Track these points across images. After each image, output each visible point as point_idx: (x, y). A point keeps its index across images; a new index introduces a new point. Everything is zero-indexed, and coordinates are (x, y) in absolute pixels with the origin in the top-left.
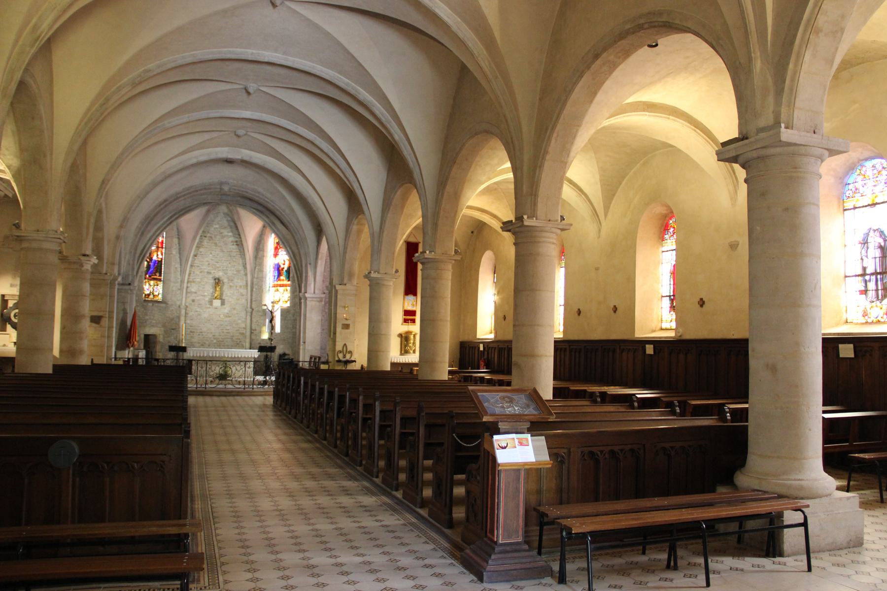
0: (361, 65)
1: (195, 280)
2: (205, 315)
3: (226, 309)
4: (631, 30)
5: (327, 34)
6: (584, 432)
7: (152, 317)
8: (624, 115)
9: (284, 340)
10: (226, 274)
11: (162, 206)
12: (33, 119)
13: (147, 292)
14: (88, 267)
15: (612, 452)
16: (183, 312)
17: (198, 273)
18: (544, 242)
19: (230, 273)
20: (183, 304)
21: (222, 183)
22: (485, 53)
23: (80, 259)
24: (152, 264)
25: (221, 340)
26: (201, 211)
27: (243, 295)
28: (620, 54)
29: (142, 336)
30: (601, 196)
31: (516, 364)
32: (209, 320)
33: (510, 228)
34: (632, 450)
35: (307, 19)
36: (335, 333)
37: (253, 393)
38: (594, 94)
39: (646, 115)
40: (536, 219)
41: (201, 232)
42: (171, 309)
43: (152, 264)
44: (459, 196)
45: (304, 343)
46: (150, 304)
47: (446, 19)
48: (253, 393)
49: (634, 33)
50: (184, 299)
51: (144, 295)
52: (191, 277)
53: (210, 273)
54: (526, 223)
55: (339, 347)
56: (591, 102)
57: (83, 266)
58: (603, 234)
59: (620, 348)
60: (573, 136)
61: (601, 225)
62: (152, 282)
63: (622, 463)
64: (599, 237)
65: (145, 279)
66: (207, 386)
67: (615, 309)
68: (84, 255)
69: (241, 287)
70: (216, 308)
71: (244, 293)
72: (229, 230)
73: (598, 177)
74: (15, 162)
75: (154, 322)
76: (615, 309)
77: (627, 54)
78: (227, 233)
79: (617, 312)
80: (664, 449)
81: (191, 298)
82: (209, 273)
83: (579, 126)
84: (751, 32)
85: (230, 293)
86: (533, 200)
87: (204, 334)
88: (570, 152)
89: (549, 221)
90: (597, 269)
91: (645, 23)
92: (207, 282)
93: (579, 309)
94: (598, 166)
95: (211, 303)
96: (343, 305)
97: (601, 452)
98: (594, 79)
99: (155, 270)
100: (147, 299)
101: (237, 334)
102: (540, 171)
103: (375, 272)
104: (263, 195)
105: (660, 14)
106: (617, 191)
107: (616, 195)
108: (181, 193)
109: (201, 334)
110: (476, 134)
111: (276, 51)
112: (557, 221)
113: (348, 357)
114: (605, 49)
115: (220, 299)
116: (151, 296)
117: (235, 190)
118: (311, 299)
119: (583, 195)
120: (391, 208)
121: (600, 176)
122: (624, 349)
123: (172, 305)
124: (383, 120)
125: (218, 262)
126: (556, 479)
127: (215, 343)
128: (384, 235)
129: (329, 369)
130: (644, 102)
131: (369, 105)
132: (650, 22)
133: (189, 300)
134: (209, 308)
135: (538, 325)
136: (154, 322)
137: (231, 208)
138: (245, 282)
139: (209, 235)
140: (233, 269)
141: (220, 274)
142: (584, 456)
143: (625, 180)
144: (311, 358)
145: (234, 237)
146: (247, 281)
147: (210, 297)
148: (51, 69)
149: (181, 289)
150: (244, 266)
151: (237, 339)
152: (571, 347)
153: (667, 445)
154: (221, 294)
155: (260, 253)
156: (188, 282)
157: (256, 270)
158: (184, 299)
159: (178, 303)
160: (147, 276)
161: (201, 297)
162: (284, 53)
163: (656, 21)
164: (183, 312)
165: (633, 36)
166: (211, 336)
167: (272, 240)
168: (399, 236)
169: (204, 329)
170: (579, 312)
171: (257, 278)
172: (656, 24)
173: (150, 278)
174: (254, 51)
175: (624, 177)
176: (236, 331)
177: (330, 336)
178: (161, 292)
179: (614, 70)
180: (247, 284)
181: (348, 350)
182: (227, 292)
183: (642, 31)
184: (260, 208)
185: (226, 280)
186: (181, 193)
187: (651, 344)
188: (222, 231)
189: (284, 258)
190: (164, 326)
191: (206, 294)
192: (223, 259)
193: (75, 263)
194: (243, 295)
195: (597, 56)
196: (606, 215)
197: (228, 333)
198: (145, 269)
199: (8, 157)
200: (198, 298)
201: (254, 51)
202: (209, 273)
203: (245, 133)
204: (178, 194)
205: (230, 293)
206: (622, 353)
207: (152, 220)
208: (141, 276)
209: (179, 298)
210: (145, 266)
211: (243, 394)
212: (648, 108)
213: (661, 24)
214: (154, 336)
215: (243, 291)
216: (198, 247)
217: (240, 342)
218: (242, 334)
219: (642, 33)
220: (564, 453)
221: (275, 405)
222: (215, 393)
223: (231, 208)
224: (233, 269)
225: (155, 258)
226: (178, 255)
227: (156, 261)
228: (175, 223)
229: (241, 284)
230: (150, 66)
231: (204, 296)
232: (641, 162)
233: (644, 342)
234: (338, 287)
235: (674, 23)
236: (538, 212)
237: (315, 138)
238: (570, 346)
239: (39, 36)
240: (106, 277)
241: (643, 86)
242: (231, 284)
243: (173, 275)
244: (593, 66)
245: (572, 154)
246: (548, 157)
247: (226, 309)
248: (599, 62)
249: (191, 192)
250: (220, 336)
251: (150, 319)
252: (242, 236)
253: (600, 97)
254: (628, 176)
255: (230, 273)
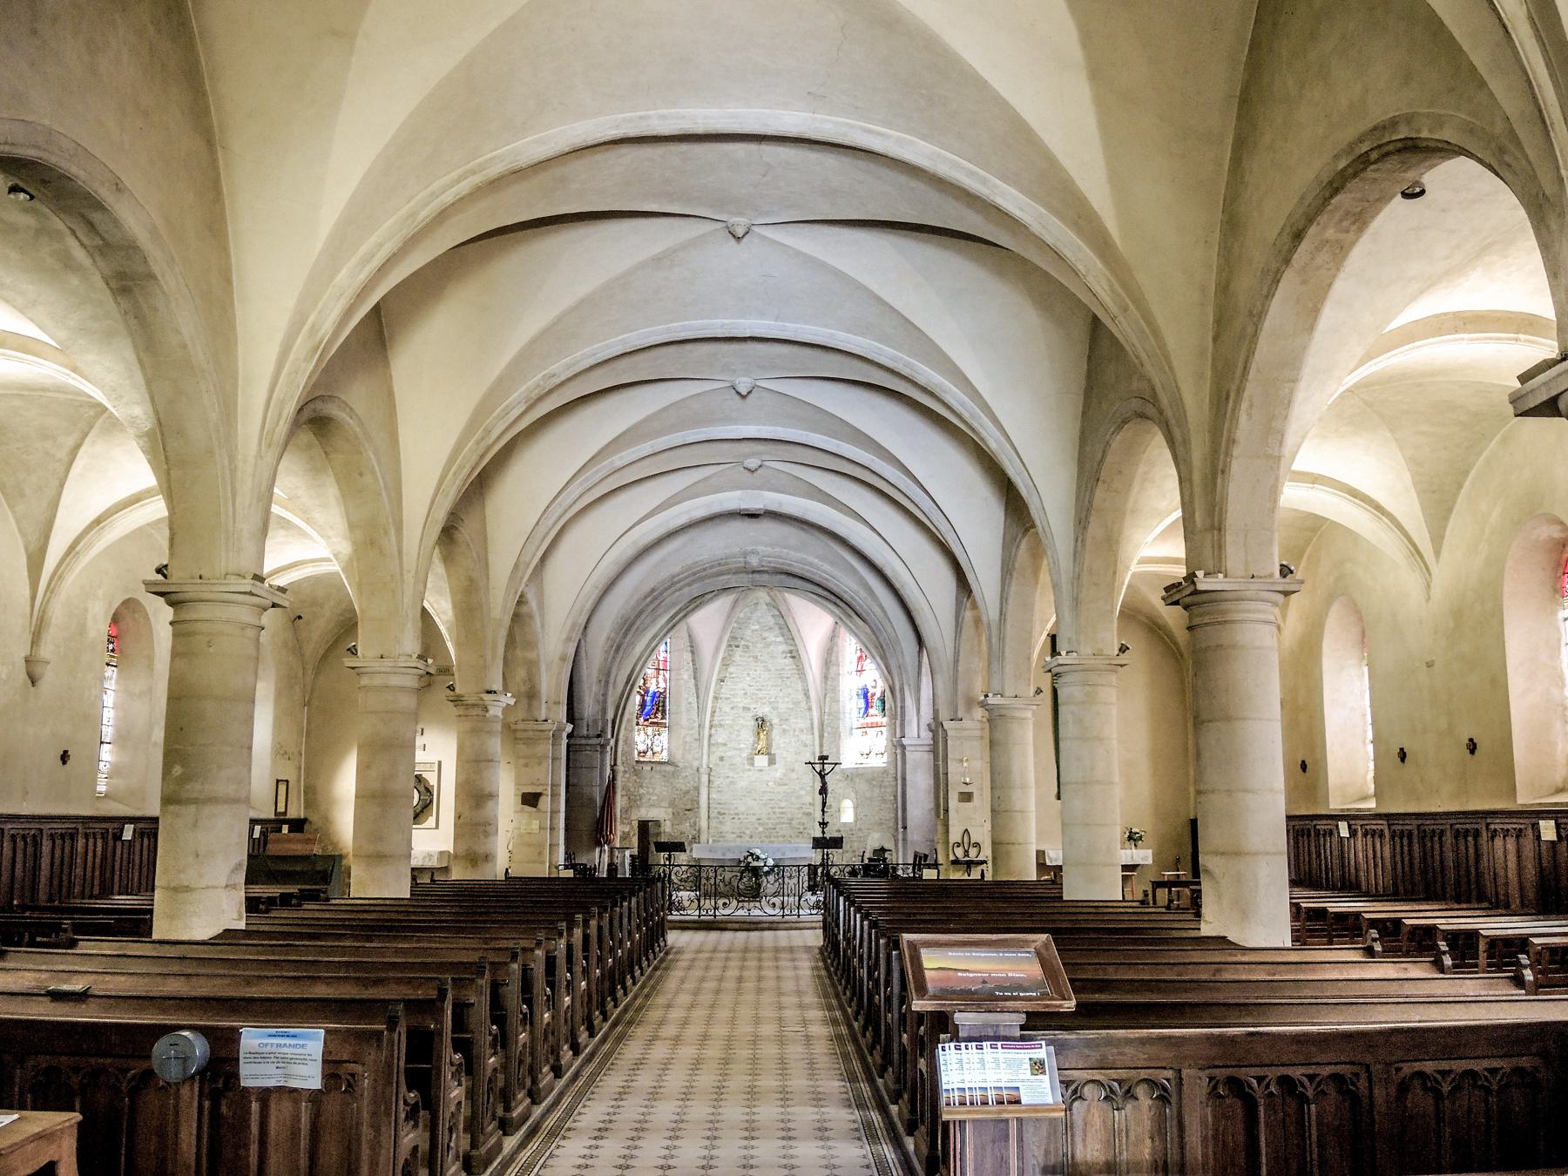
0: (907, 320)
1: (722, 723)
2: (743, 784)
3: (778, 771)
4: (1350, 171)
5: (839, 274)
6: (1212, 1034)
7: (651, 790)
8: (1411, 345)
9: (881, 824)
10: (775, 708)
11: (649, 600)
12: (361, 475)
13: (642, 747)
14: (496, 711)
15: (1285, 1081)
16: (705, 779)
17: (727, 710)
18: (1241, 621)
19: (782, 707)
20: (705, 766)
21: (745, 554)
22: (1100, 265)
23: (482, 699)
24: (648, 699)
25: (771, 826)
26: (724, 602)
27: (806, 746)
28: (1345, 224)
29: (635, 824)
30: (1421, 516)
31: (1207, 871)
32: (750, 792)
33: (1177, 597)
34: (1335, 1077)
35: (798, 253)
36: (946, 811)
37: (797, 925)
38: (1315, 312)
39: (1463, 339)
40: (1226, 576)
41: (726, 638)
42: (683, 774)
43: (648, 699)
44: (1118, 542)
45: (905, 828)
46: (647, 768)
47: (1017, 213)
48: (797, 925)
49: (1355, 175)
50: (705, 757)
51: (636, 752)
52: (716, 718)
53: (749, 709)
54: (1201, 587)
55: (955, 836)
56: (1311, 328)
57: (487, 711)
58: (1437, 592)
59: (1487, 829)
60: (1286, 402)
61: (1430, 574)
62: (650, 730)
63: (1313, 1107)
64: (1428, 599)
65: (638, 724)
66: (717, 913)
67: (1472, 747)
68: (489, 692)
69: (802, 730)
70: (761, 770)
71: (807, 742)
72: (777, 631)
73: (1407, 477)
74: (345, 548)
75: (655, 798)
76: (1472, 747)
77: (1360, 220)
78: (774, 637)
79: (1476, 752)
80: (1421, 1075)
81: (719, 754)
82: (746, 709)
83: (1295, 381)
84: (1552, 124)
85: (784, 743)
86: (1216, 538)
87: (741, 816)
88: (1283, 435)
89: (1253, 577)
90: (1430, 665)
91: (1371, 150)
92: (743, 726)
93: (1402, 749)
94: (1404, 456)
95: (751, 760)
96: (958, 757)
97: (1260, 1079)
98: (1304, 282)
99: (655, 708)
100: (642, 759)
101: (800, 816)
102: (1223, 480)
103: (995, 694)
104: (818, 569)
105: (1393, 123)
106: (1454, 502)
107: (1454, 512)
108: (678, 575)
109: (737, 817)
110: (1125, 422)
111: (762, 315)
112: (1271, 575)
113: (973, 853)
114: (1310, 220)
115: (767, 754)
116: (650, 753)
117: (770, 562)
118: (913, 749)
119: (1384, 518)
120: (1015, 574)
121: (1412, 477)
122: (1495, 830)
123: (685, 767)
124: (966, 415)
125: (760, 690)
126: (1152, 1138)
127: (760, 833)
128: (1008, 627)
129: (938, 880)
130: (1454, 313)
131: (937, 392)
132: (1379, 146)
133: (714, 758)
134: (749, 770)
135: (1246, 791)
136: (655, 798)
137: (772, 594)
138: (809, 722)
139: (743, 643)
140: (787, 699)
141: (764, 710)
142: (1215, 1088)
143: (1470, 477)
144: (915, 857)
145: (786, 643)
146: (812, 720)
147: (750, 751)
148: (391, 394)
149: (699, 740)
150: (805, 694)
151: (799, 824)
152: (1492, 827)
153: (1429, 1067)
154: (769, 746)
155: (833, 670)
156: (711, 727)
157: (828, 699)
158: (705, 757)
159: (696, 764)
160: (642, 719)
161: (734, 752)
162: (777, 319)
163: (1390, 142)
164: (705, 779)
165: (1357, 180)
166: (753, 819)
167: (850, 646)
168: (1037, 627)
169: (742, 809)
170: (1403, 755)
171: (829, 714)
172: (1391, 148)
173: (646, 723)
174: (726, 321)
175: (1466, 473)
176: (798, 809)
177: (938, 817)
178: (666, 746)
179: (1345, 257)
180: (812, 724)
181: (972, 842)
182: (779, 741)
183: (1372, 167)
184: (820, 591)
185: (775, 721)
186: (678, 575)
187: (1551, 819)
188: (766, 634)
189: (873, 677)
190: (672, 804)
191: (742, 746)
192: (770, 683)
193: (474, 705)
194: (806, 746)
195: (1298, 236)
196: (1437, 553)
197: (782, 813)
198: (637, 708)
199: (335, 540)
200: (729, 754)
201: (726, 321)
202: (746, 709)
203: (760, 463)
204: (674, 577)
205: (784, 743)
206: (1493, 838)
207: (631, 625)
208: (629, 720)
209: (696, 756)
210: (637, 703)
211: (781, 926)
212: (1465, 324)
213: (1399, 145)
214: (657, 823)
215: (807, 738)
216: (725, 665)
217: (805, 829)
218: (809, 814)
219: (1372, 171)
220: (1168, 1080)
221: (822, 950)
222: (729, 925)
223: (772, 594)
224: (787, 699)
225: (653, 688)
226: (693, 681)
227: (655, 693)
228: (682, 626)
229: (802, 726)
230: (553, 368)
231: (740, 749)
232: (1498, 438)
233: (1535, 815)
234: (947, 725)
235: (1420, 138)
236: (1228, 563)
237: (873, 460)
238: (1389, 825)
239: (320, 343)
240: (545, 726)
241: (1430, 284)
242: (784, 726)
243: (684, 717)
244: (1295, 256)
245: (1290, 440)
246: (1236, 451)
247: (778, 771)
248: (1305, 246)
249: (697, 574)
250: (769, 819)
251: (648, 793)
252: (798, 641)
253: (1329, 315)
254: (1475, 468)
255: (782, 707)
